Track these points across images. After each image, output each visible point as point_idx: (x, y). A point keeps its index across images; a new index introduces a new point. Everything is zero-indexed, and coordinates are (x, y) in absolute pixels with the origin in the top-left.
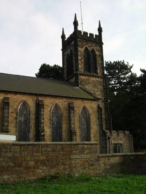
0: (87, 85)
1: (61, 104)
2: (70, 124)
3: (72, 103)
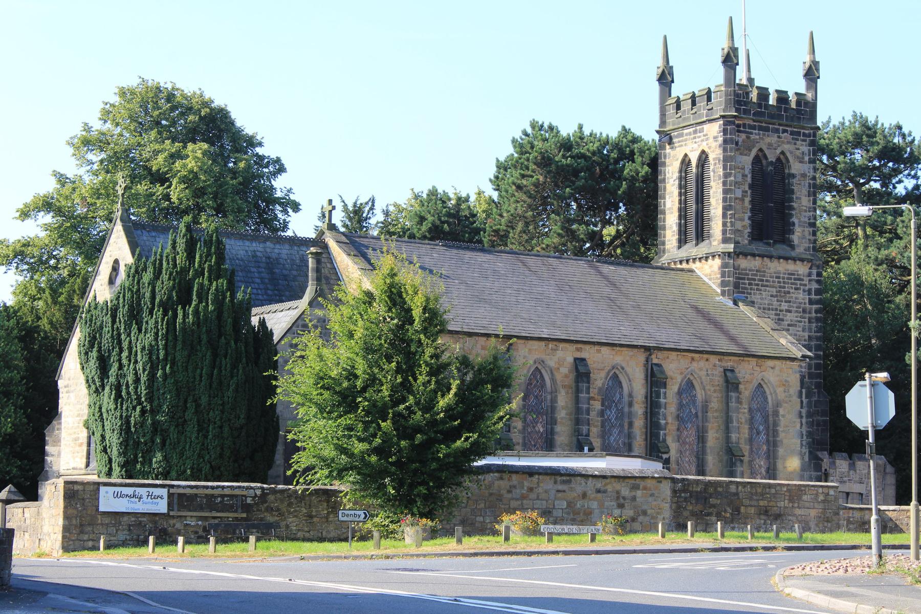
0: (758, 290)
1: (704, 373)
2: (727, 430)
3: (732, 371)
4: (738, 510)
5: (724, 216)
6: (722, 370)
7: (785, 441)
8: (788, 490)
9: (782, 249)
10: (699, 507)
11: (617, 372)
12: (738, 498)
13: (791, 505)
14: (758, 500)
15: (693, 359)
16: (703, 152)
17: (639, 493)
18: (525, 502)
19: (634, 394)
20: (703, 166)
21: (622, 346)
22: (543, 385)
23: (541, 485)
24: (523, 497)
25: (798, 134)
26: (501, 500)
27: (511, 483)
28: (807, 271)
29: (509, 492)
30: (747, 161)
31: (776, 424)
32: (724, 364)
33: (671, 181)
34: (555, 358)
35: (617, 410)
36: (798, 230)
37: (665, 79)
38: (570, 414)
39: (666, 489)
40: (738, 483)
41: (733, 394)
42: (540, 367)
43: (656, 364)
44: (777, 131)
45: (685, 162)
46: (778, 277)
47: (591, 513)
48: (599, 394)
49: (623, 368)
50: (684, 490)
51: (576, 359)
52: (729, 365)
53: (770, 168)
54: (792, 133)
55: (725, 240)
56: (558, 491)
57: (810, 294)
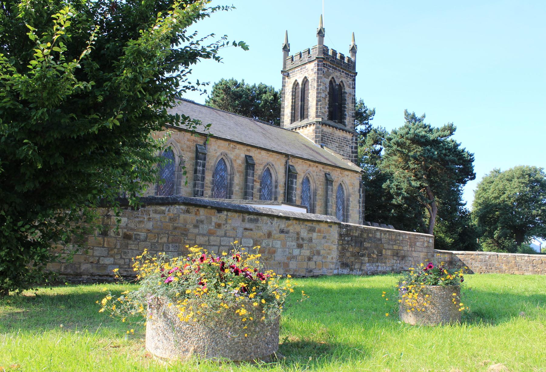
4: (381, 253)
5: (317, 104)
6: (324, 173)
7: (352, 215)
8: (410, 238)
9: (340, 126)
10: (357, 249)
11: (270, 167)
12: (381, 243)
13: (410, 249)
14: (393, 245)
15: (310, 165)
16: (306, 77)
17: (315, 235)
18: (212, 238)
19: (278, 181)
20: (305, 85)
21: (273, 151)
22: (225, 169)
23: (229, 222)
24: (211, 233)
25: (348, 75)
26: (186, 235)
27: (198, 218)
28: (351, 138)
29: (196, 226)
30: (327, 81)
31: (348, 206)
32: (325, 170)
33: (288, 93)
34: (234, 154)
35: (269, 190)
36: (348, 118)
37: (286, 49)
38: (242, 189)
39: (334, 232)
40: (381, 231)
41: (329, 187)
42: (224, 158)
43: (291, 165)
44: (340, 71)
45: (296, 84)
46: (339, 139)
47: (274, 252)
48: (259, 178)
49: (273, 165)
50: (347, 235)
51: (246, 156)
52: (327, 171)
53: (337, 87)
54: (346, 74)
55: (317, 116)
56: (246, 229)
57: (352, 148)
